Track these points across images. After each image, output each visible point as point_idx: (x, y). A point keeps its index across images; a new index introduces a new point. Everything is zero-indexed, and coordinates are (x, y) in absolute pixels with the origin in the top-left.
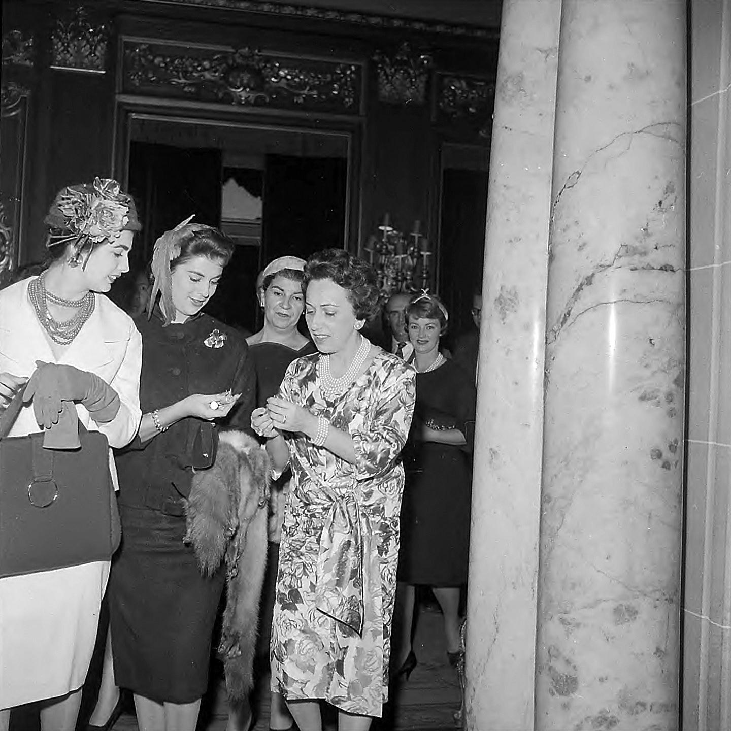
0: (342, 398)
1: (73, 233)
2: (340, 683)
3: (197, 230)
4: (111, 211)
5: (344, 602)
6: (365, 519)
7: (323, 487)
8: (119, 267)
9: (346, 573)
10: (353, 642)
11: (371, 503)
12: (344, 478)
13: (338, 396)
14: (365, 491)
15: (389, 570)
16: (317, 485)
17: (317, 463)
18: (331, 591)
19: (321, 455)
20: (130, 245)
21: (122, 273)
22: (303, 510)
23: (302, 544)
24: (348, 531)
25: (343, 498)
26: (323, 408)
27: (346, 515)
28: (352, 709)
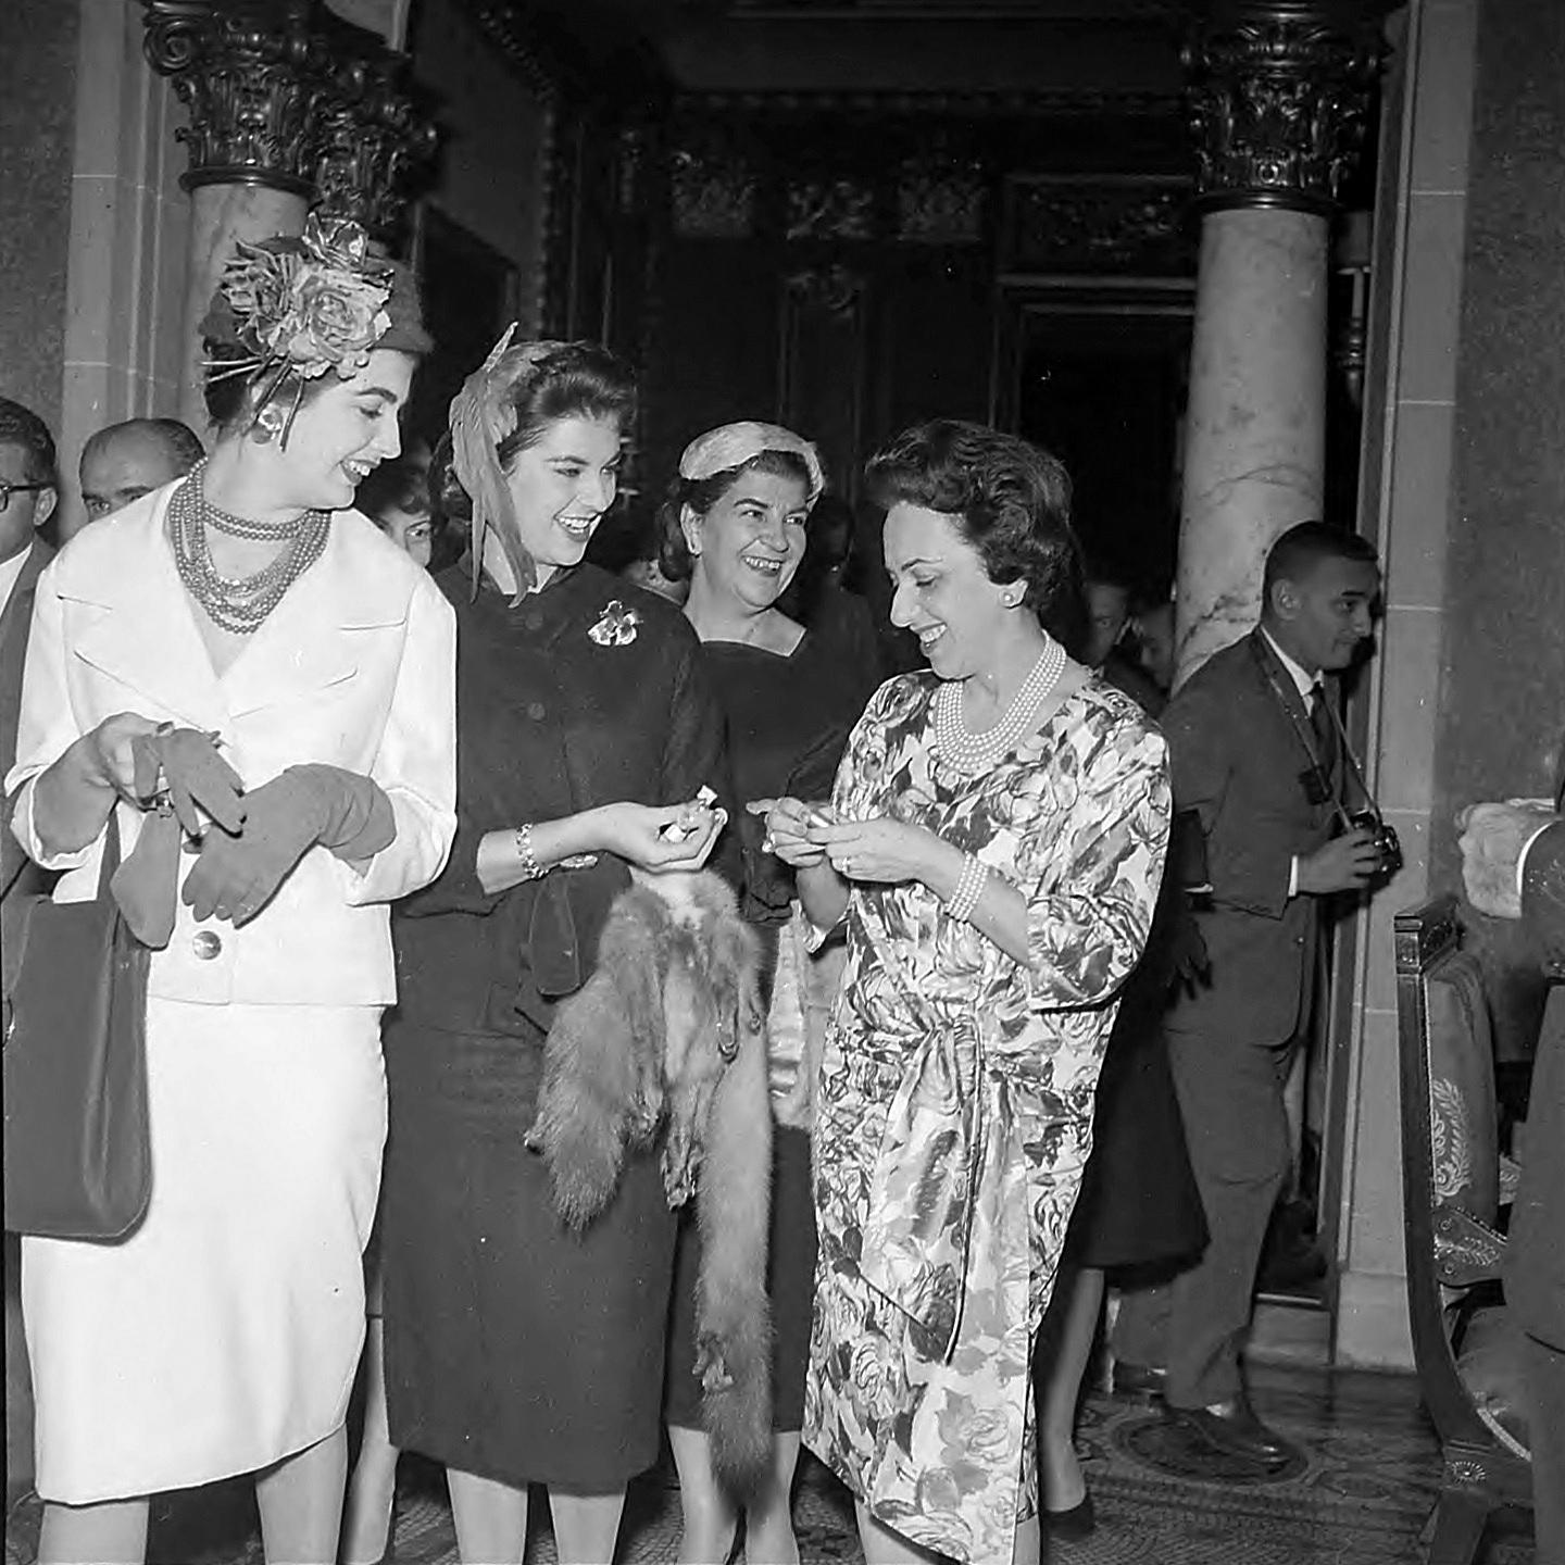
0: (976, 785)
1: (252, 355)
2: (899, 1469)
3: (543, 356)
4: (343, 298)
5: (927, 1275)
6: (998, 1084)
7: (909, 994)
8: (374, 444)
9: (938, 1207)
10: (942, 1378)
11: (1018, 1050)
12: (956, 980)
13: (965, 779)
14: (1006, 1019)
15: (1055, 1202)
16: (895, 985)
17: (900, 933)
18: (900, 1244)
19: (908, 915)
20: (402, 392)
21: (383, 460)
22: (859, 1039)
23: (855, 1121)
24: (951, 1110)
25: (949, 1027)
26: (927, 802)
27: (952, 1070)
28: (923, 1537)
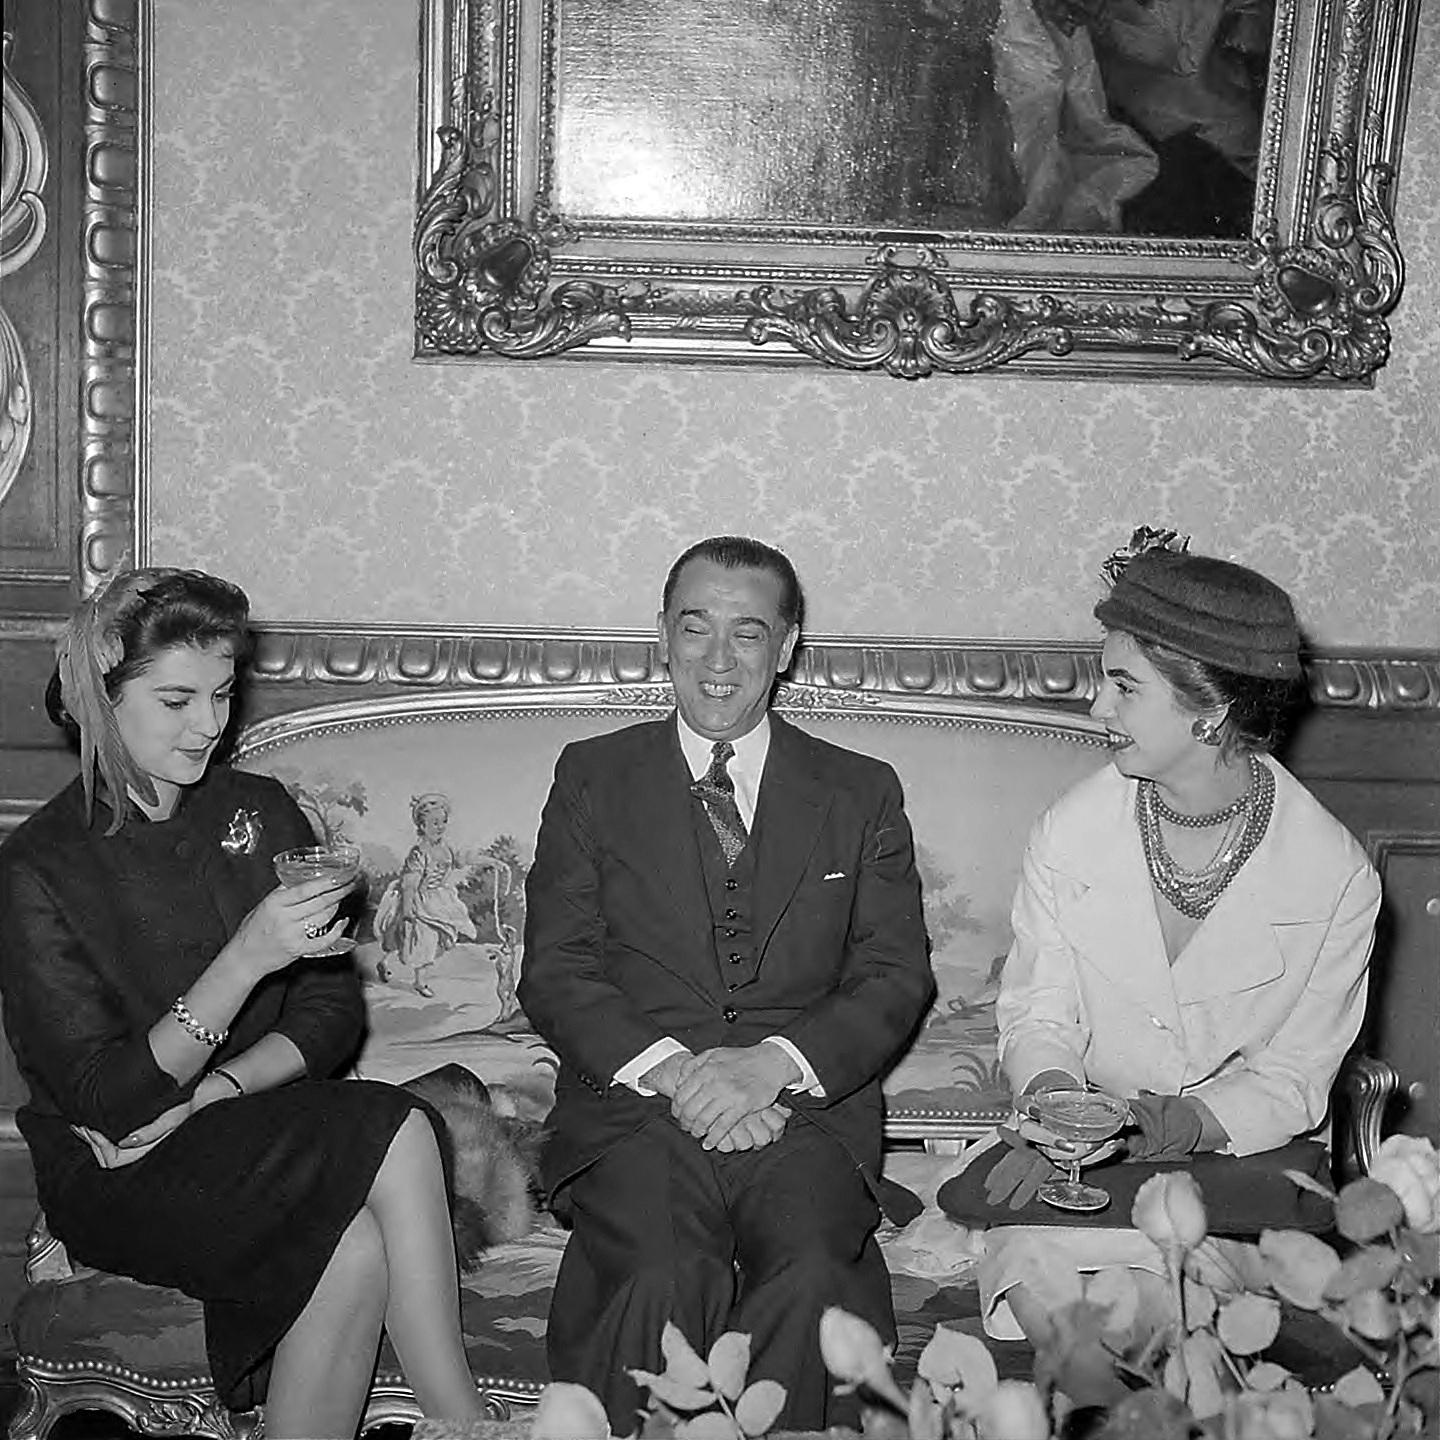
3: (149, 587)
